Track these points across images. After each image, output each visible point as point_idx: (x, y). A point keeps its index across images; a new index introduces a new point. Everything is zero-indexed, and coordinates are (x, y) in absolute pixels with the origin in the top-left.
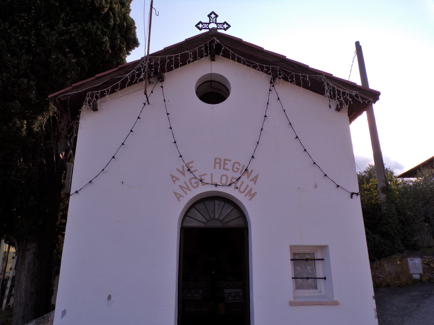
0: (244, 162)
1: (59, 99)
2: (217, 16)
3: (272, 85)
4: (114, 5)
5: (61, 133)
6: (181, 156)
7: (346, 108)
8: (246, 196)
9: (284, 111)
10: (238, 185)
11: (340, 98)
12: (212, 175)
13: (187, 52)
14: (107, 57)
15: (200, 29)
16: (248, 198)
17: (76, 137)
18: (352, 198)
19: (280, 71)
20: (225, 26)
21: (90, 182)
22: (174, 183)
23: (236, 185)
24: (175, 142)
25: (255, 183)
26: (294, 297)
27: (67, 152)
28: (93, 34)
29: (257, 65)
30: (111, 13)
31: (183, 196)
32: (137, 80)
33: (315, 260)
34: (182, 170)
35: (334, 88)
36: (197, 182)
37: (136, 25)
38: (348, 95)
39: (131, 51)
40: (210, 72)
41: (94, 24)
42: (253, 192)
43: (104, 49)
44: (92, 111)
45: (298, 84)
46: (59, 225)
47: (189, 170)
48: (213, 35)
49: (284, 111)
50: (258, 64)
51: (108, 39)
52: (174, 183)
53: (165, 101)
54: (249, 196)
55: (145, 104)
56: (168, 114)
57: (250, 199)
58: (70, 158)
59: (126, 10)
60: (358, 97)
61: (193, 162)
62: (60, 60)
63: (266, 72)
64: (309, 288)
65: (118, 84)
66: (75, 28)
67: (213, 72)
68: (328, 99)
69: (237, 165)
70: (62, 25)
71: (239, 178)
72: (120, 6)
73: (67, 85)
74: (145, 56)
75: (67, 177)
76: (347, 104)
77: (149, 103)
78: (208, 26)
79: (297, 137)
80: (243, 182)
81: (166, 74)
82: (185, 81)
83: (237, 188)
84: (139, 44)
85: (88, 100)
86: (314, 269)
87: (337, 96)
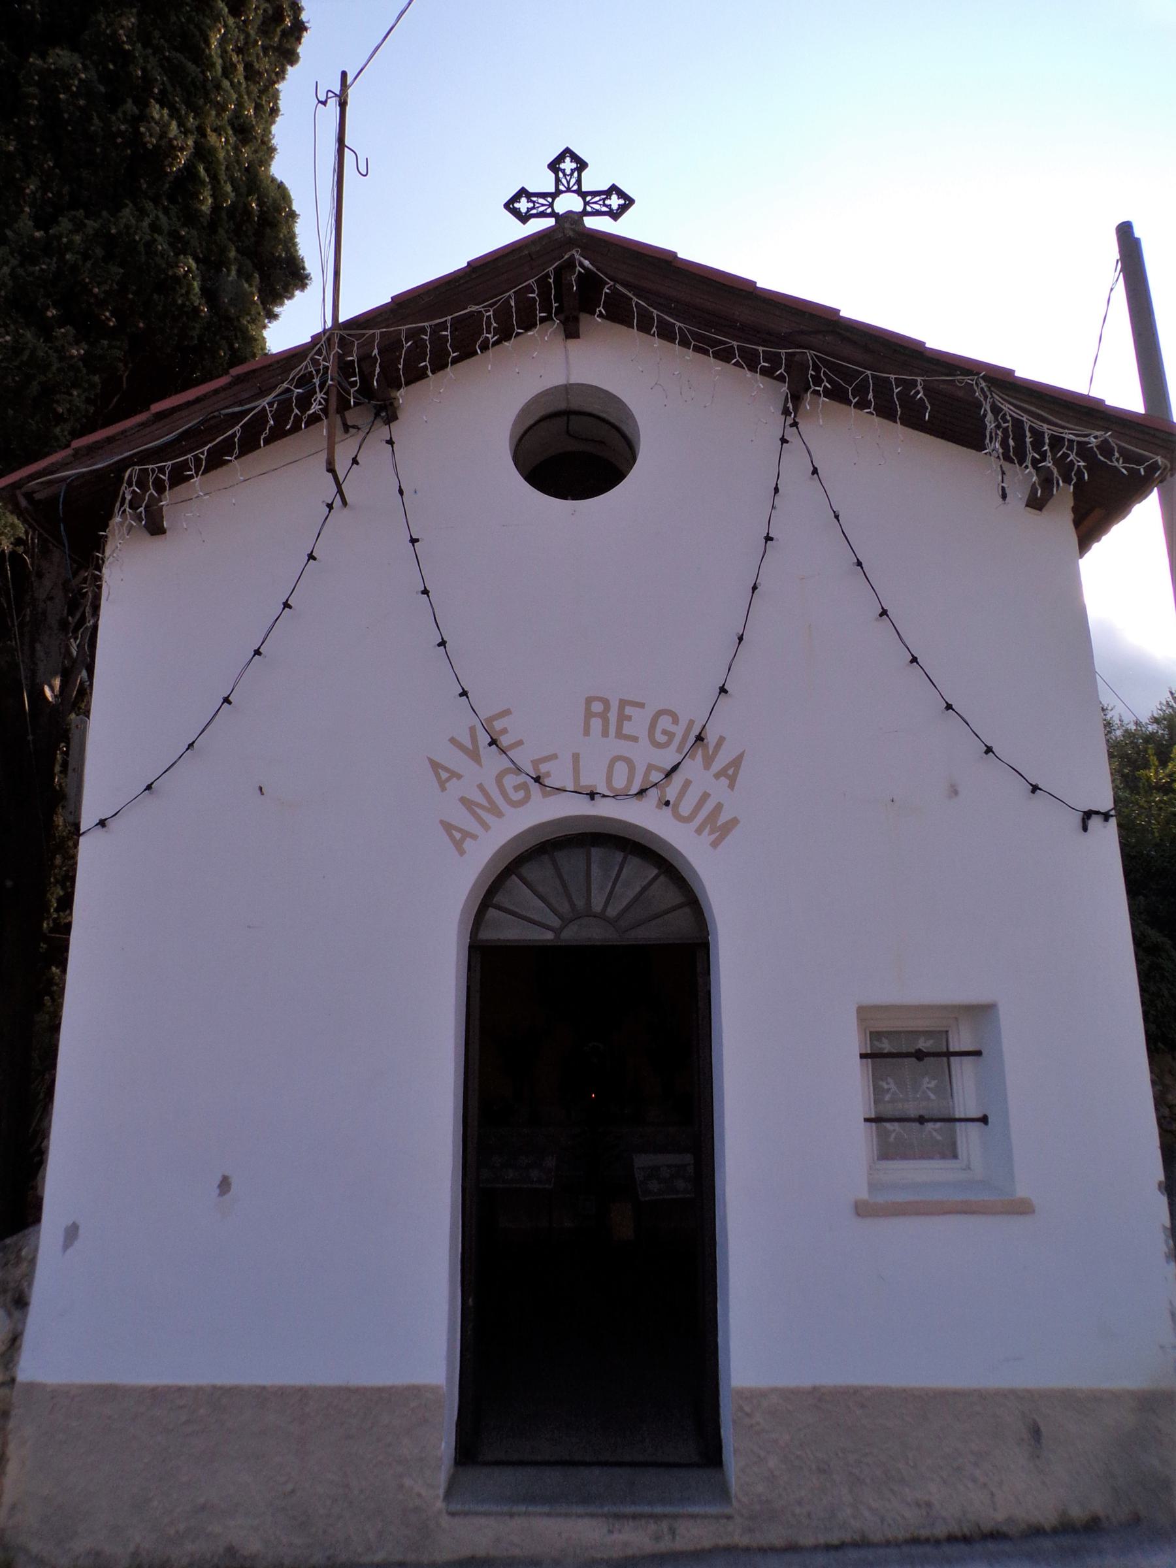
0: (693, 710)
1: (29, 496)
2: (582, 165)
3: (790, 420)
4: (212, 138)
5: (44, 613)
6: (464, 693)
7: (1064, 495)
8: (699, 831)
9: (837, 517)
10: (671, 793)
11: (1044, 459)
12: (576, 757)
13: (475, 308)
14: (195, 333)
15: (524, 218)
16: (707, 838)
17: (95, 628)
18: (1085, 829)
19: (816, 368)
20: (615, 202)
21: (149, 787)
22: (443, 789)
23: (663, 793)
24: (443, 643)
25: (732, 786)
26: (873, 1186)
27: (67, 676)
28: (142, 249)
29: (732, 347)
30: (201, 169)
31: (474, 837)
32: (298, 420)
33: (949, 1054)
34: (467, 742)
35: (1018, 424)
36: (524, 786)
37: (294, 207)
38: (1070, 448)
39: (282, 304)
40: (560, 380)
41: (142, 213)
42: (723, 818)
43: (183, 305)
44: (147, 535)
45: (886, 412)
46: (51, 931)
47: (493, 742)
48: (570, 243)
49: (837, 517)
50: (735, 344)
51: (194, 265)
52: (443, 789)
53: (401, 492)
54: (712, 832)
55: (330, 506)
56: (414, 541)
57: (715, 844)
58: (78, 699)
59: (256, 152)
60: (1108, 453)
61: (506, 713)
62: (27, 353)
63: (765, 372)
64: (925, 1156)
65: (234, 435)
66: (77, 231)
67: (572, 381)
68: (995, 464)
69: (665, 722)
70: (30, 223)
71: (675, 768)
72: (232, 140)
73: (57, 439)
74: (325, 331)
75: (70, 768)
76: (1067, 481)
77: (345, 503)
78: (551, 205)
79: (884, 613)
80: (687, 783)
81: (402, 396)
82: (476, 412)
83: (667, 803)
84: (307, 277)
85: (128, 497)
86: (946, 1089)
87: (1031, 454)
